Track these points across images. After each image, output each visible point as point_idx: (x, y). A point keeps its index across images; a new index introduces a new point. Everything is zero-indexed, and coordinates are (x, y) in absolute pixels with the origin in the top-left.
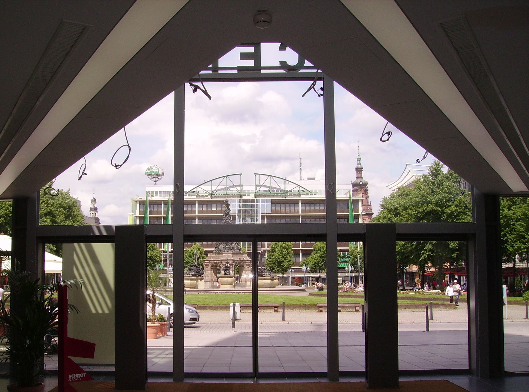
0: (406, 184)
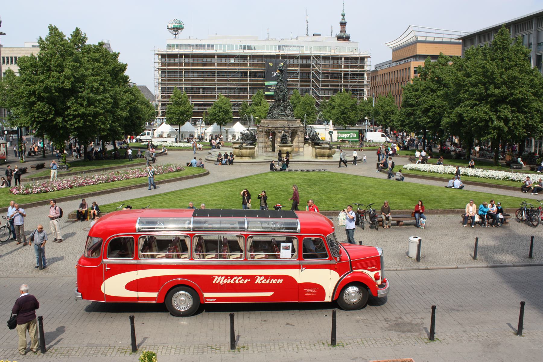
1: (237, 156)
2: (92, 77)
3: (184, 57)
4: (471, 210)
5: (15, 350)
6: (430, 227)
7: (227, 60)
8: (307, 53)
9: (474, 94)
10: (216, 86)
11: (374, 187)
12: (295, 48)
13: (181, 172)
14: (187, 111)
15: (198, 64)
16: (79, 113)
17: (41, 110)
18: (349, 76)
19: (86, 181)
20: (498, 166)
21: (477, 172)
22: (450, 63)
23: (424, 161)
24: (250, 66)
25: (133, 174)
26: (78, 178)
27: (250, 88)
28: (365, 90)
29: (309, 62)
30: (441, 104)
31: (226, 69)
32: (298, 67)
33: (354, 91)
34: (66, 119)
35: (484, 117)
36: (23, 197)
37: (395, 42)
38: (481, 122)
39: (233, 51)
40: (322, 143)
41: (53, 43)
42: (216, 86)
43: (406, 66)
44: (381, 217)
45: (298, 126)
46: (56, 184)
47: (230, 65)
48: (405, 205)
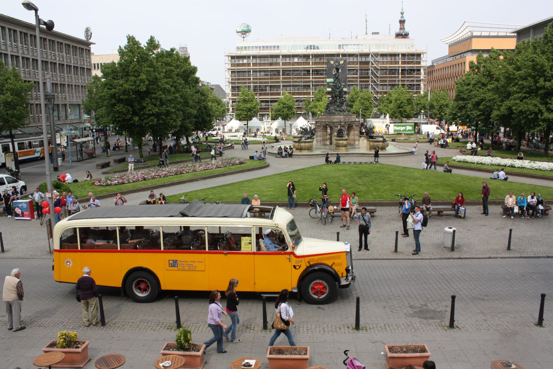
0: (465, 36)
1: (297, 149)
2: (166, 80)
3: (251, 57)
4: (510, 201)
5: (81, 322)
6: (470, 218)
7: (291, 60)
8: (366, 51)
9: (523, 88)
10: (282, 84)
11: (421, 179)
12: (354, 47)
13: (243, 165)
14: (254, 108)
15: (264, 64)
16: (153, 112)
17: (120, 111)
18: (406, 72)
19: (157, 174)
20: (548, 157)
21: (524, 164)
22: (501, 57)
23: (474, 152)
24: (312, 64)
25: (200, 167)
26: (150, 171)
27: (313, 85)
28: (421, 85)
29: (368, 59)
30: (491, 98)
31: (290, 68)
32: (357, 64)
33: (411, 86)
34: (142, 118)
35: (533, 110)
36: (103, 188)
37: (451, 37)
38: (531, 114)
39: (296, 51)
40: (376, 137)
41: (131, 51)
42: (282, 84)
43: (461, 61)
44: (422, 208)
45: (354, 120)
46: (131, 177)
47: (294, 64)
48: (448, 197)
